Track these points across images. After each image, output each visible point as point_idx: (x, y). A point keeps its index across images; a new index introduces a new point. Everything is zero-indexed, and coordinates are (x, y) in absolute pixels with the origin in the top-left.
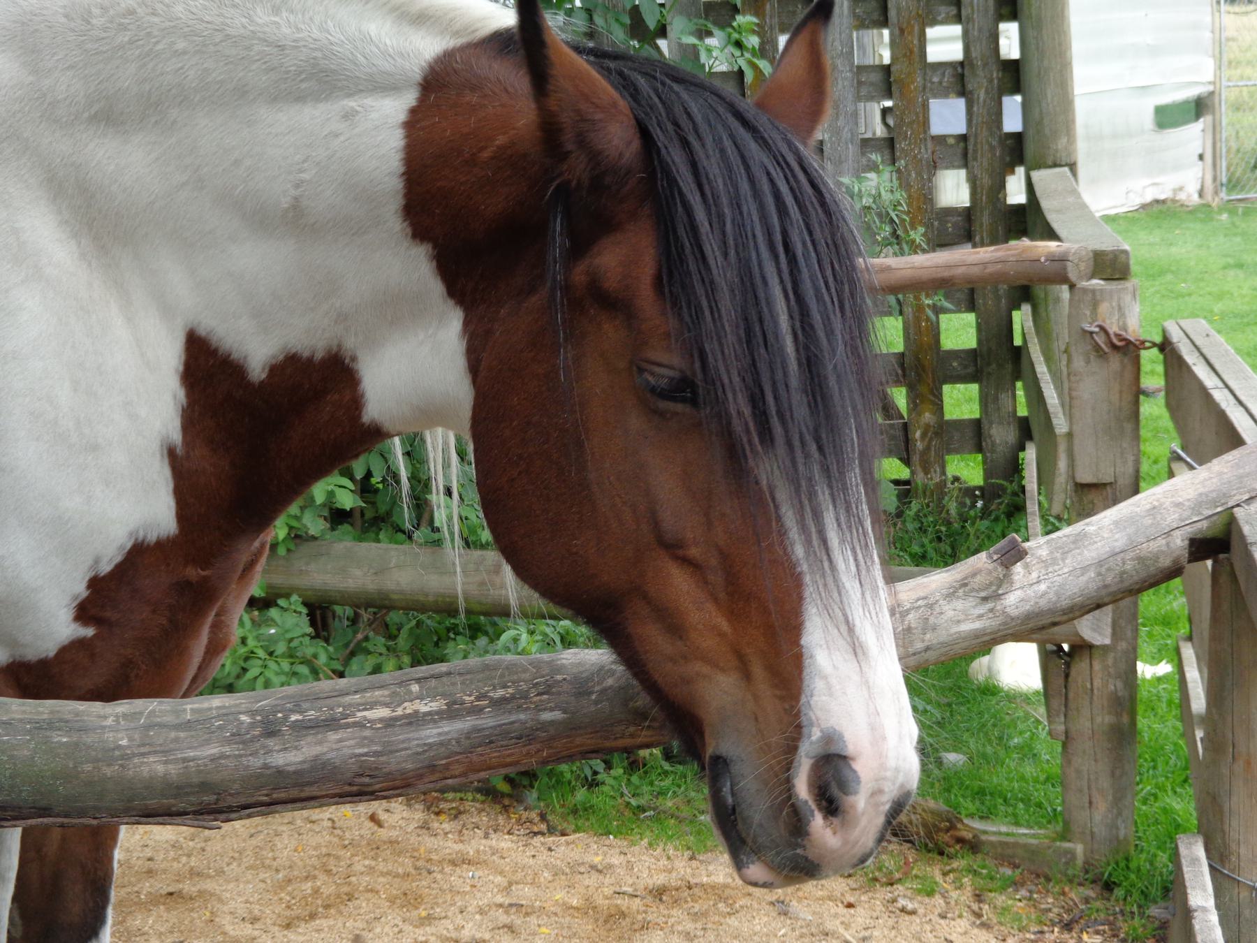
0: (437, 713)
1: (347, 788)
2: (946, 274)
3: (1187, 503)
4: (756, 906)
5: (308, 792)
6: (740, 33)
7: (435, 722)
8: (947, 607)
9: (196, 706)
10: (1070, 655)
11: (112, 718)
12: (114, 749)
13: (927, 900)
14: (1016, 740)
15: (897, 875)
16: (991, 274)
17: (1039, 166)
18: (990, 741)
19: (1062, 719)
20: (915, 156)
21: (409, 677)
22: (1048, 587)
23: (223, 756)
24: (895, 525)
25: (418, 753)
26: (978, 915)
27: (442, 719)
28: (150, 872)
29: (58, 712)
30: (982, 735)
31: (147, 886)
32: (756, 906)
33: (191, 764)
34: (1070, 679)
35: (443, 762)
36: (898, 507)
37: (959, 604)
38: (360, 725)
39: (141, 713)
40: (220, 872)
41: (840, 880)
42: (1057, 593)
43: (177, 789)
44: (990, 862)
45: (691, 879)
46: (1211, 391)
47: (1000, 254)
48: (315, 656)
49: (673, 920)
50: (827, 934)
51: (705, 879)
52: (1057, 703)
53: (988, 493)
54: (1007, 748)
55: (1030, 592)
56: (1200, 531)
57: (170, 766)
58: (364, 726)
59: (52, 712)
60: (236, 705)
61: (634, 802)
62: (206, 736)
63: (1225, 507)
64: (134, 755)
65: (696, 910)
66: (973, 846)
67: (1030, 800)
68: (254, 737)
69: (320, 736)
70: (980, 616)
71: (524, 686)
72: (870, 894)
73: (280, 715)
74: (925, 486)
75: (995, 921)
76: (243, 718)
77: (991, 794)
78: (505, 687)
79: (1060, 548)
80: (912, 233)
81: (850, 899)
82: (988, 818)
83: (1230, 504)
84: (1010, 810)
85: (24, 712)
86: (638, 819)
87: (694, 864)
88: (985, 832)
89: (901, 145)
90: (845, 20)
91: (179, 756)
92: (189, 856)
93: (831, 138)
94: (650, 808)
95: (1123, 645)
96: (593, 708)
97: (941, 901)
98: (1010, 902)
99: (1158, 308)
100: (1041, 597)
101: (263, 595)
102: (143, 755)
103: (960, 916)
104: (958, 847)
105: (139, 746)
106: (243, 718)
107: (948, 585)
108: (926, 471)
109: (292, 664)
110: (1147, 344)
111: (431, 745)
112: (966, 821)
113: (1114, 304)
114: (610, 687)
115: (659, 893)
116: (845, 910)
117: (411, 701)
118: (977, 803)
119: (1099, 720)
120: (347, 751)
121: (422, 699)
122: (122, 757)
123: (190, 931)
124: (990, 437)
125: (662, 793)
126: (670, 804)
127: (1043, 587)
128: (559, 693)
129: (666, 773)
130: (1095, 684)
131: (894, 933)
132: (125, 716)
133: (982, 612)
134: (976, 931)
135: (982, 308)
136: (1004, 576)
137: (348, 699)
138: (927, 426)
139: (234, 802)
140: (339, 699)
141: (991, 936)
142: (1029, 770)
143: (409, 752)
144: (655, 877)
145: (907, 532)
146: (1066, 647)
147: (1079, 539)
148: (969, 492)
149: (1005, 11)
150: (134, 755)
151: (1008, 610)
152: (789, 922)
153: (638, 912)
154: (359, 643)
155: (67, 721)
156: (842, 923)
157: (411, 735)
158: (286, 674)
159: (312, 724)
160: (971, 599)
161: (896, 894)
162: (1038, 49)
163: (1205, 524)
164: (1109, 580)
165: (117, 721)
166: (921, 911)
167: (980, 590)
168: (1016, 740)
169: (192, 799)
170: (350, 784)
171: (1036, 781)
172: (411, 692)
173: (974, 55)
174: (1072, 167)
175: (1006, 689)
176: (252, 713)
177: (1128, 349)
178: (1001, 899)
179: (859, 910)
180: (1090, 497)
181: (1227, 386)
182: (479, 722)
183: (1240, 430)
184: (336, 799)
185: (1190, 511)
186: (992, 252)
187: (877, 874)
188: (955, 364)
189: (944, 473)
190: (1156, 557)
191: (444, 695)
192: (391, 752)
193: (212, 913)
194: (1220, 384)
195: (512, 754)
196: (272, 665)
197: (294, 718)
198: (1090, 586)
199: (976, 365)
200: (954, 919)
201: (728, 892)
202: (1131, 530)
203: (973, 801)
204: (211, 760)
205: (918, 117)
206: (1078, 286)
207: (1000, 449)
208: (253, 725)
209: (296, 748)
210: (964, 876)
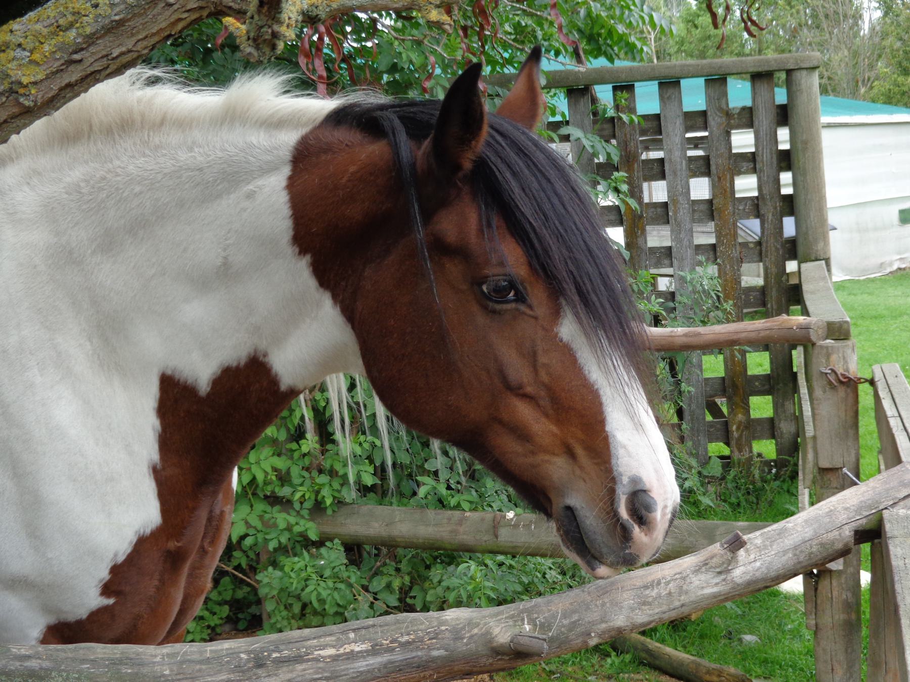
0: (366, 651)
2: (735, 337)
3: (852, 508)
6: (616, 183)
7: (364, 657)
8: (694, 579)
9: (213, 648)
10: (818, 576)
11: (160, 657)
14: (789, 627)
16: (762, 337)
17: (806, 261)
19: (814, 617)
20: (729, 255)
21: (348, 628)
22: (762, 564)
24: (721, 485)
25: (353, 678)
27: (368, 655)
29: (126, 653)
30: (768, 623)
34: (818, 591)
36: (722, 474)
37: (703, 577)
38: (316, 660)
39: (178, 653)
42: (767, 568)
46: (889, 419)
47: (768, 324)
48: (349, 577)
52: (811, 606)
53: (779, 464)
54: (783, 632)
55: (749, 568)
56: (862, 525)
58: (319, 660)
59: (122, 653)
60: (239, 647)
62: (219, 668)
63: (877, 509)
67: (796, 666)
68: (249, 668)
69: (291, 667)
70: (717, 584)
71: (420, 634)
73: (266, 654)
74: (739, 460)
76: (243, 656)
77: (772, 662)
78: (408, 634)
80: (725, 304)
82: (769, 678)
83: (881, 508)
85: (105, 653)
86: (550, 679)
89: (720, 249)
90: (684, 173)
93: (676, 245)
94: (558, 673)
95: (851, 570)
99: (897, 338)
100: (757, 571)
101: (318, 539)
106: (243, 656)
107: (695, 565)
108: (740, 451)
109: (335, 582)
110: (862, 380)
111: (361, 672)
113: (840, 355)
114: (476, 634)
117: (349, 644)
118: (763, 668)
119: (837, 617)
121: (356, 643)
124: (780, 429)
126: (570, 669)
127: (758, 564)
130: (834, 594)
132: (168, 655)
133: (718, 581)
135: (773, 349)
136: (732, 558)
137: (309, 643)
138: (740, 422)
140: (304, 643)
142: (797, 646)
145: (728, 489)
146: (815, 571)
147: (782, 533)
148: (767, 463)
149: (783, 165)
154: (378, 568)
155: (131, 659)
157: (349, 666)
158: (331, 589)
159: (286, 660)
160: (710, 573)
162: (804, 188)
163: (864, 521)
164: (801, 559)
165: (163, 659)
167: (716, 567)
168: (789, 627)
171: (800, 653)
172: (349, 638)
173: (764, 192)
174: (827, 261)
175: (785, 592)
176: (248, 652)
177: (850, 384)
180: (829, 476)
181: (900, 416)
182: (392, 657)
183: (900, 449)
185: (854, 513)
186: (763, 323)
188: (757, 384)
189: (751, 451)
190: (833, 543)
191: (370, 640)
192: (337, 677)
194: (897, 414)
196: (322, 584)
197: (274, 655)
198: (789, 563)
199: (770, 385)
202: (815, 526)
205: (730, 231)
206: (818, 344)
207: (786, 436)
208: (248, 661)
209: (276, 675)
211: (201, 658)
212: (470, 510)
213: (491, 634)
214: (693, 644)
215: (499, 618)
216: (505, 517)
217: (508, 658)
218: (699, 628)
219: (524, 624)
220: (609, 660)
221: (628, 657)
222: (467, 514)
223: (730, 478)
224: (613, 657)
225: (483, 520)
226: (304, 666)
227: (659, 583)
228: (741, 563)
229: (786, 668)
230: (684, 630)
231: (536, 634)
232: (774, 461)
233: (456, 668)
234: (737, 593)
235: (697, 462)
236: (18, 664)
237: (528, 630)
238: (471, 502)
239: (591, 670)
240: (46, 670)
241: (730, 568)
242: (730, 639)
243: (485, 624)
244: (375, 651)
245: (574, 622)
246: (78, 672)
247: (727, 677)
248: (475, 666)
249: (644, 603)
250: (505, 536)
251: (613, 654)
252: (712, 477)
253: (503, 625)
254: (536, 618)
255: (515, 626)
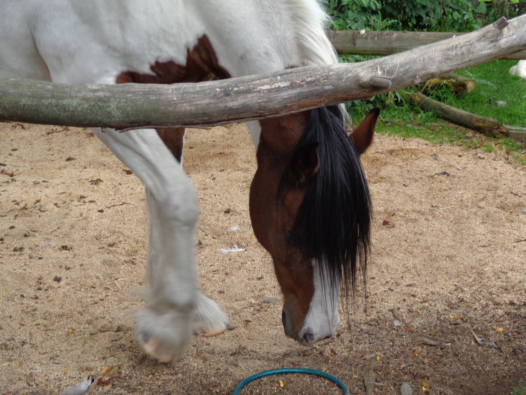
0: (288, 87)
1: (255, 115)
4: (426, 156)
5: (241, 116)
7: (286, 90)
8: (477, 45)
9: (201, 85)
12: (171, 101)
13: (489, 154)
15: (478, 145)
18: (515, 96)
23: (210, 103)
24: (485, 18)
25: (280, 102)
26: (507, 159)
27: (288, 89)
28: (214, 146)
29: (152, 88)
31: (213, 151)
32: (426, 156)
33: (199, 106)
35: (289, 105)
37: (482, 44)
38: (259, 92)
39: (181, 88)
40: (238, 146)
41: (457, 147)
42: (520, 39)
43: (195, 115)
44: (513, 140)
45: (403, 147)
49: (396, 161)
50: (451, 166)
51: (408, 147)
55: (510, 39)
57: (192, 107)
59: (149, 88)
60: (215, 85)
61: (384, 120)
62: (204, 96)
64: (179, 103)
65: (404, 158)
66: (507, 134)
69: (245, 96)
70: (490, 48)
72: (468, 152)
75: (513, 161)
77: (514, 116)
78: (311, 77)
79: (522, 22)
81: (461, 154)
82: (513, 124)
84: (521, 121)
85: (140, 88)
87: (404, 141)
88: (511, 130)
91: (195, 103)
92: (227, 140)
94: (390, 122)
96: (343, 84)
97: (494, 154)
98: (519, 155)
100: (514, 40)
102: (182, 103)
103: (501, 160)
104: (501, 135)
105: (180, 100)
106: (217, 89)
111: (285, 99)
112: (504, 126)
114: (350, 77)
115: (391, 152)
116: (458, 158)
118: (509, 119)
120: (255, 101)
121: (281, 82)
122: (174, 104)
123: (227, 166)
125: (394, 117)
126: (397, 121)
128: (331, 79)
129: (396, 110)
131: (475, 165)
132: (175, 89)
134: (506, 165)
136: (500, 33)
137: (255, 82)
139: (216, 120)
141: (511, 167)
143: (277, 101)
144: (390, 146)
150: (179, 103)
151: (501, 45)
152: (437, 162)
153: (383, 159)
155: (155, 91)
156: (457, 162)
159: (242, 91)
161: (477, 152)
165: (173, 91)
166: (486, 158)
169: (200, 119)
170: (256, 113)
172: (277, 80)
178: (516, 154)
179: (463, 158)
184: (252, 118)
187: (471, 145)
191: (289, 80)
192: (271, 101)
193: (234, 160)
195: (314, 102)
197: (235, 89)
200: (498, 161)
201: (416, 151)
203: (508, 118)
204: (206, 105)
208: (220, 92)
209: (236, 100)
210: (503, 145)
211: (194, 91)
212: (339, 30)
213: (359, 76)
214: (468, 106)
215: (363, 67)
216: (360, 33)
217: (368, 90)
218: (472, 97)
219: (377, 71)
220: (419, 116)
221: (430, 114)
222: (338, 32)
223: (491, 14)
224: (422, 114)
225: (347, 35)
226: (252, 95)
227: (456, 47)
228: (505, 36)
229: (522, 118)
230: (464, 98)
231: (385, 76)
232: (518, 4)
233: (339, 96)
234: (502, 54)
235: (472, 4)
236: (92, 94)
237: (380, 74)
238: (340, 25)
239: (409, 121)
240: (108, 97)
241: (498, 39)
242: (490, 103)
243: (355, 71)
244: (292, 86)
245: (407, 70)
246: (126, 98)
247: (489, 123)
248: (349, 95)
249: (448, 59)
250: (360, 44)
251: (422, 112)
252: (481, 13)
253: (366, 71)
254: (385, 68)
255: (373, 72)
